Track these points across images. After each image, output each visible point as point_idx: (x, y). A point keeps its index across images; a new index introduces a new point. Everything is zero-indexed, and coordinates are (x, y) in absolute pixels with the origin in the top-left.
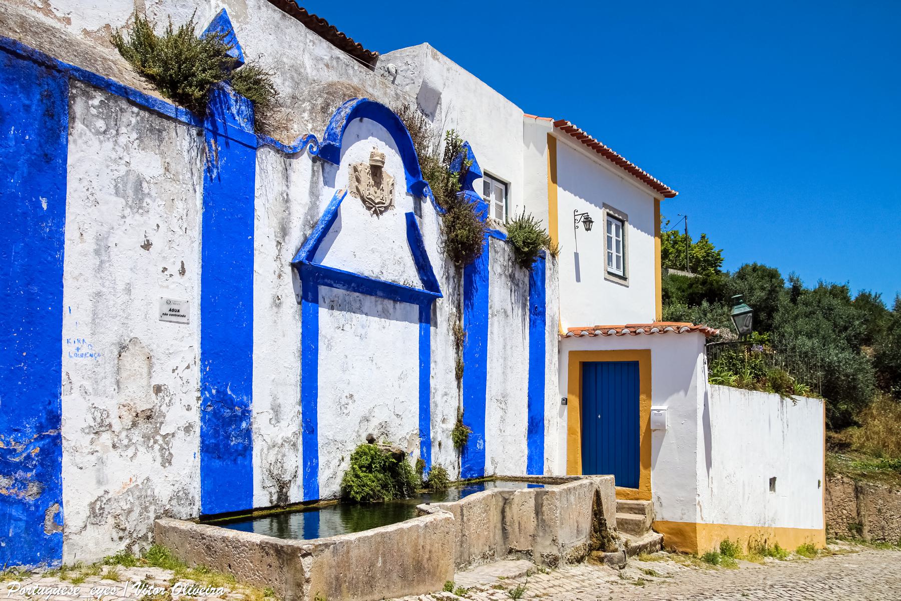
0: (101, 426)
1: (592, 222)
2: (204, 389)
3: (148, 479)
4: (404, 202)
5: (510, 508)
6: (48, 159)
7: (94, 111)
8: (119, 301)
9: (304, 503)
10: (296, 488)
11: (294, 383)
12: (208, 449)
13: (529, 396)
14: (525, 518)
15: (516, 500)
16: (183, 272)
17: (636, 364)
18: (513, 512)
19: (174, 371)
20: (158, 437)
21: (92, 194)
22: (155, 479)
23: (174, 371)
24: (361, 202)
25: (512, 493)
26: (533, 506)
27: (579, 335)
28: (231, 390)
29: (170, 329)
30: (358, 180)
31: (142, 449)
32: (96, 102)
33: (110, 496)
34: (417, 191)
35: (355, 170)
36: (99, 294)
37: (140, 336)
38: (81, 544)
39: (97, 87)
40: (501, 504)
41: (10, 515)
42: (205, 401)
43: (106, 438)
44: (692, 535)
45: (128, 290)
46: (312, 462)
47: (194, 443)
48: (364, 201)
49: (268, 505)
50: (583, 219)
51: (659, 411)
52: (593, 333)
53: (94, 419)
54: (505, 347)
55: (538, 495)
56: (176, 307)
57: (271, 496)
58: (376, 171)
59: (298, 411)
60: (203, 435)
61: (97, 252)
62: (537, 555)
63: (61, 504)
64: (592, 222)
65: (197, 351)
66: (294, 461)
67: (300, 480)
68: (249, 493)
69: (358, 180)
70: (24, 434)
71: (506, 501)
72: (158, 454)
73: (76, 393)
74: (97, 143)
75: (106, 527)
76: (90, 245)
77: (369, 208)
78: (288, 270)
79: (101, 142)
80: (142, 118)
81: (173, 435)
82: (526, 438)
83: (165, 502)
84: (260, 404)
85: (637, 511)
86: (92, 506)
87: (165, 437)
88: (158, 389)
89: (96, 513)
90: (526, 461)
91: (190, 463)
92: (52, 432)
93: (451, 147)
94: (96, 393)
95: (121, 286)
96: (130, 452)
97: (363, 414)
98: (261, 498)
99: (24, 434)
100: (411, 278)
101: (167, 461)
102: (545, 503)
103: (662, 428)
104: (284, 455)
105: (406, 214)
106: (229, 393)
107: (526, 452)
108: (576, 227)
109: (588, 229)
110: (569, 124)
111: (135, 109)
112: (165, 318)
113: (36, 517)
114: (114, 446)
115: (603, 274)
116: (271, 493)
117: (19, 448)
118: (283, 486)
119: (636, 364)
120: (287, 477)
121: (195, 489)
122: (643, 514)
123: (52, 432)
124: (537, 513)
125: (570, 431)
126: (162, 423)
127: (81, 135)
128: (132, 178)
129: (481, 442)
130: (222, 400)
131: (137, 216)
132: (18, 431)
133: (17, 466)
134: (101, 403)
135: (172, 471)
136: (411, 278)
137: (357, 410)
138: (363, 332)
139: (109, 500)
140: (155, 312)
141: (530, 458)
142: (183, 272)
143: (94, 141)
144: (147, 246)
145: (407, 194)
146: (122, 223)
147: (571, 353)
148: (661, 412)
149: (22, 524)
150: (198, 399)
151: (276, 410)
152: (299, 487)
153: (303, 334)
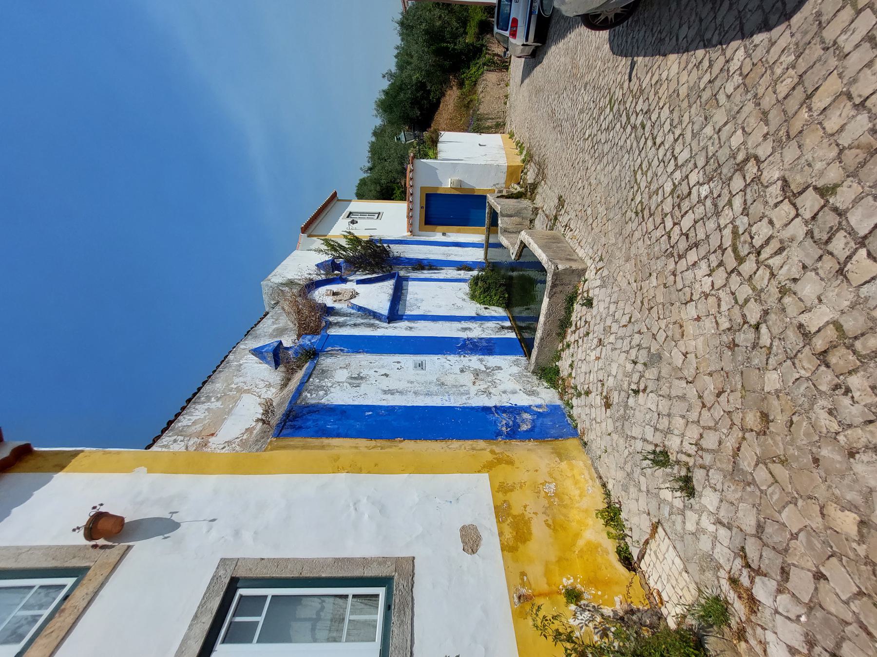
3: (510, 375)
7: (314, 395)
15: (505, 226)
16: (398, 362)
17: (427, 195)
25: (501, 228)
27: (411, 225)
30: (341, 300)
31: (495, 377)
32: (309, 395)
35: (335, 301)
37: (436, 377)
44: (513, 168)
45: (412, 382)
50: (352, 225)
52: (410, 217)
55: (503, 216)
56: (418, 365)
58: (335, 294)
60: (483, 355)
62: (532, 217)
65: (439, 356)
66: (491, 324)
67: (500, 322)
69: (341, 300)
71: (505, 231)
72: (496, 371)
73: (469, 401)
76: (389, 397)
77: (355, 297)
78: (391, 325)
79: (331, 393)
80: (316, 377)
81: (485, 366)
84: (464, 335)
86: (529, 395)
87: (487, 369)
91: (499, 360)
92: (494, 409)
103: (460, 181)
105: (357, 284)
107: (471, 248)
111: (311, 380)
112: (424, 367)
115: (378, 221)
119: (427, 195)
123: (494, 409)
124: (512, 217)
128: (350, 381)
132: (495, 422)
137: (460, 303)
141: (473, 247)
142: (398, 362)
144: (386, 375)
147: (420, 230)
150: (464, 356)
151: (465, 329)
153: (424, 320)
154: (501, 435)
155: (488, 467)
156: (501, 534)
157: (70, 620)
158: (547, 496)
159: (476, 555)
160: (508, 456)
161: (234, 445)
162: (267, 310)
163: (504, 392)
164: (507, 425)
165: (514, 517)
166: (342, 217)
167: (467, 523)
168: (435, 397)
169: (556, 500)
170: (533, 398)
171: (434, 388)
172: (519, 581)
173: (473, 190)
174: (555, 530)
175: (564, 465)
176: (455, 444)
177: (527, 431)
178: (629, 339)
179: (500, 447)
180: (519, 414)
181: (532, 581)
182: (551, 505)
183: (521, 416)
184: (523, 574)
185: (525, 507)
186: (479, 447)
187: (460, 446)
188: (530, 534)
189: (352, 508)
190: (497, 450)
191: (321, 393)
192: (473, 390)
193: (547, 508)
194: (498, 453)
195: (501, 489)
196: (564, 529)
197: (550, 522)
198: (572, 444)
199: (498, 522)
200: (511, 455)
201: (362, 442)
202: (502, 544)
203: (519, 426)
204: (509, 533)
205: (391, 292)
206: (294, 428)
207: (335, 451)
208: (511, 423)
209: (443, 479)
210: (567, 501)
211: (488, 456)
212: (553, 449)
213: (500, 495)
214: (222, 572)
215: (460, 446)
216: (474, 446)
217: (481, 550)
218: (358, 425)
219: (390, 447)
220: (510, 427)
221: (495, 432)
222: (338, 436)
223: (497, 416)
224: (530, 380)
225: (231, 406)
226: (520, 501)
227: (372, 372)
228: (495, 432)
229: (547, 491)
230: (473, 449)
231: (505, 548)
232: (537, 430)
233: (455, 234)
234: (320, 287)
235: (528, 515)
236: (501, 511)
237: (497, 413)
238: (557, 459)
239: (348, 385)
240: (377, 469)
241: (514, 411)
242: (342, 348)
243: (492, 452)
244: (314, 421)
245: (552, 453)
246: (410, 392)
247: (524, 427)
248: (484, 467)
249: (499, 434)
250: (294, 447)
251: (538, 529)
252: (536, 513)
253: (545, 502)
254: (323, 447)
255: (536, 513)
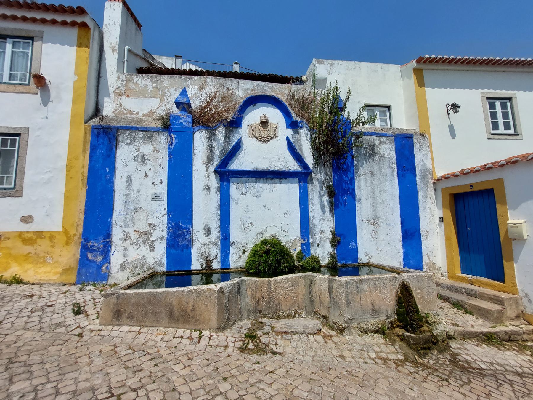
0: (126, 238)
1: (459, 107)
2: (168, 223)
4: (285, 132)
5: (314, 286)
6: (109, 156)
7: (126, 138)
8: (135, 196)
9: (221, 269)
10: (216, 263)
11: (216, 219)
12: (170, 246)
13: (401, 217)
14: (323, 294)
15: (317, 282)
16: (161, 183)
18: (316, 289)
19: (157, 218)
20: (149, 241)
21: (125, 163)
22: (147, 256)
23: (157, 218)
24: (256, 139)
25: (315, 277)
26: (327, 287)
28: (181, 223)
29: (157, 202)
33: (128, 261)
34: (294, 126)
36: (128, 195)
38: (116, 277)
39: (127, 130)
40: (309, 283)
41: (91, 265)
42: (169, 227)
43: (128, 242)
45: (138, 192)
46: (226, 251)
47: (164, 244)
48: (257, 138)
49: (201, 269)
51: (515, 224)
52: (464, 173)
53: (124, 235)
54: (373, 192)
57: (202, 266)
59: (219, 231)
60: (168, 240)
61: (127, 181)
63: (109, 263)
64: (459, 107)
66: (215, 251)
67: (219, 259)
68: (190, 263)
70: (98, 240)
71: (312, 281)
72: (148, 247)
74: (127, 147)
75: (126, 272)
76: (125, 179)
79: (128, 146)
80: (144, 135)
81: (155, 241)
82: (401, 242)
83: (151, 264)
85: (496, 302)
86: (121, 265)
87: (152, 242)
88: (150, 224)
89: (123, 267)
90: (402, 255)
92: (108, 240)
93: (331, 98)
94: (125, 226)
95: (135, 191)
96: (137, 246)
97: (260, 231)
98: (196, 265)
99: (98, 240)
100: (293, 166)
101: (152, 250)
102: (334, 286)
104: (210, 249)
106: (181, 224)
107: (402, 250)
108: (449, 114)
109: (456, 112)
110: (427, 56)
111: (142, 132)
113: (100, 267)
114: (131, 244)
115: (485, 135)
116: (202, 264)
117: (96, 245)
118: (209, 261)
120: (211, 258)
121: (164, 260)
122: (502, 305)
123: (108, 240)
125: (448, 239)
126: (151, 236)
127: (121, 146)
128: (140, 155)
129: (354, 244)
130: (178, 226)
131: (143, 167)
132: (97, 239)
133: (95, 250)
134: (126, 230)
135: (154, 254)
136: (293, 166)
138: (258, 194)
139: (128, 263)
140: (150, 198)
142: (161, 183)
143: (126, 146)
145: (287, 128)
146: (136, 170)
147: (443, 190)
148: (517, 225)
149: (95, 269)
152: (218, 262)
153: (220, 199)
154: (85, 241)
155: (65, 231)
156: (28, 232)
157: (11, 90)
158: (44, 257)
159: (19, 221)
160: (71, 243)
161: (119, 109)
162: (304, 78)
163: (125, 249)
164: (92, 246)
165: (36, 239)
166: (480, 91)
167: (34, 219)
168: (123, 207)
169: (42, 261)
170: (118, 267)
171: (132, 206)
172: (7, 236)
173: (511, 259)
174: (26, 256)
175: (60, 270)
176: (82, 216)
177: (87, 256)
178: (43, 333)
179: (78, 239)
180: (102, 254)
181: (6, 241)
182: (40, 258)
183: (99, 255)
184: (9, 238)
185: (40, 245)
186: (78, 228)
187: (80, 219)
188: (26, 245)
189: (47, 170)
190: (76, 238)
191: (129, 141)
192: (130, 230)
193: (38, 255)
194: (74, 238)
195: (52, 237)
196: (25, 260)
197: (30, 255)
198: (73, 278)
199: (34, 232)
200: (72, 244)
201: (86, 170)
202: (23, 232)
203: (91, 253)
204: (27, 236)
205: (292, 170)
206: (98, 134)
207: (81, 157)
208: (95, 248)
209: (60, 209)
210: (39, 265)
211: (72, 232)
212: (73, 268)
213: (48, 235)
214: (23, 129)
215: (80, 219)
216: (80, 226)
217: (21, 223)
218: (98, 165)
219: (83, 183)
220: (91, 247)
221: (88, 238)
222: (91, 157)
223: (102, 241)
224: (137, 269)
225: (150, 96)
226: (44, 245)
227: (149, 166)
228: (88, 238)
229: (48, 257)
230: (78, 225)
231: (21, 234)
232: (87, 262)
233: (443, 233)
234: (279, 109)
235: (35, 246)
236: (40, 235)
237: (104, 242)
238: (65, 268)
239: (136, 155)
240: (69, 178)
241: (106, 251)
242: (173, 145)
243: (75, 235)
244: (103, 143)
245: (70, 266)
246: (129, 191)
247: (90, 256)
248: (66, 230)
249: (87, 240)
250: (85, 137)
251: (28, 249)
252: (36, 249)
253: (42, 255)
254: (84, 151)
255: (36, 249)
